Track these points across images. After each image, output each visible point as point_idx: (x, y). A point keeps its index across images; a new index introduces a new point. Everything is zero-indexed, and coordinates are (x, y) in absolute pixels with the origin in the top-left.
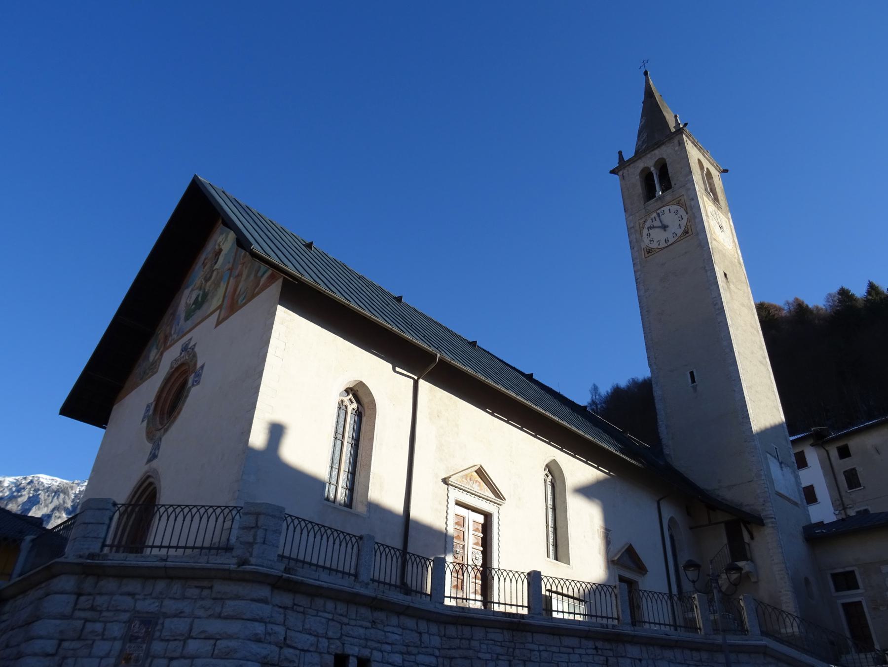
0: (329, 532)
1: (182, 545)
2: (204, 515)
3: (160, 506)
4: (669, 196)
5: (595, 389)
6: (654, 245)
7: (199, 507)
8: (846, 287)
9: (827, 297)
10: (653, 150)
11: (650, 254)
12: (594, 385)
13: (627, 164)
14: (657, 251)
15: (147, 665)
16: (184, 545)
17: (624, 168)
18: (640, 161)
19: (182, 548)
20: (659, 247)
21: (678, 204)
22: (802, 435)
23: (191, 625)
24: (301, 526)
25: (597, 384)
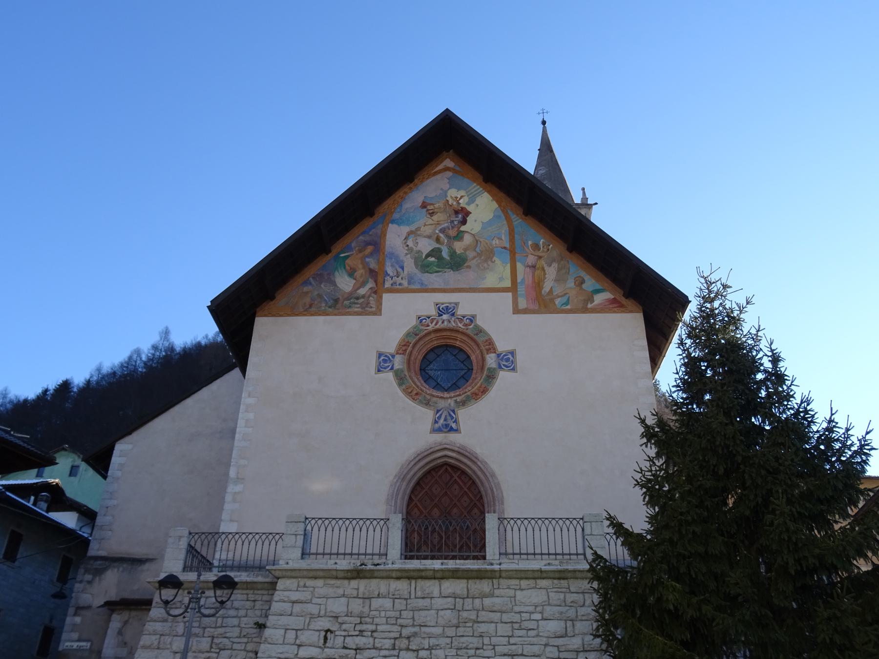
0: (568, 522)
1: (314, 552)
2: (266, 540)
3: (220, 534)
5: (166, 333)
7: (247, 534)
12: (167, 328)
15: (109, 647)
16: (322, 552)
24: (566, 525)
25: (170, 328)
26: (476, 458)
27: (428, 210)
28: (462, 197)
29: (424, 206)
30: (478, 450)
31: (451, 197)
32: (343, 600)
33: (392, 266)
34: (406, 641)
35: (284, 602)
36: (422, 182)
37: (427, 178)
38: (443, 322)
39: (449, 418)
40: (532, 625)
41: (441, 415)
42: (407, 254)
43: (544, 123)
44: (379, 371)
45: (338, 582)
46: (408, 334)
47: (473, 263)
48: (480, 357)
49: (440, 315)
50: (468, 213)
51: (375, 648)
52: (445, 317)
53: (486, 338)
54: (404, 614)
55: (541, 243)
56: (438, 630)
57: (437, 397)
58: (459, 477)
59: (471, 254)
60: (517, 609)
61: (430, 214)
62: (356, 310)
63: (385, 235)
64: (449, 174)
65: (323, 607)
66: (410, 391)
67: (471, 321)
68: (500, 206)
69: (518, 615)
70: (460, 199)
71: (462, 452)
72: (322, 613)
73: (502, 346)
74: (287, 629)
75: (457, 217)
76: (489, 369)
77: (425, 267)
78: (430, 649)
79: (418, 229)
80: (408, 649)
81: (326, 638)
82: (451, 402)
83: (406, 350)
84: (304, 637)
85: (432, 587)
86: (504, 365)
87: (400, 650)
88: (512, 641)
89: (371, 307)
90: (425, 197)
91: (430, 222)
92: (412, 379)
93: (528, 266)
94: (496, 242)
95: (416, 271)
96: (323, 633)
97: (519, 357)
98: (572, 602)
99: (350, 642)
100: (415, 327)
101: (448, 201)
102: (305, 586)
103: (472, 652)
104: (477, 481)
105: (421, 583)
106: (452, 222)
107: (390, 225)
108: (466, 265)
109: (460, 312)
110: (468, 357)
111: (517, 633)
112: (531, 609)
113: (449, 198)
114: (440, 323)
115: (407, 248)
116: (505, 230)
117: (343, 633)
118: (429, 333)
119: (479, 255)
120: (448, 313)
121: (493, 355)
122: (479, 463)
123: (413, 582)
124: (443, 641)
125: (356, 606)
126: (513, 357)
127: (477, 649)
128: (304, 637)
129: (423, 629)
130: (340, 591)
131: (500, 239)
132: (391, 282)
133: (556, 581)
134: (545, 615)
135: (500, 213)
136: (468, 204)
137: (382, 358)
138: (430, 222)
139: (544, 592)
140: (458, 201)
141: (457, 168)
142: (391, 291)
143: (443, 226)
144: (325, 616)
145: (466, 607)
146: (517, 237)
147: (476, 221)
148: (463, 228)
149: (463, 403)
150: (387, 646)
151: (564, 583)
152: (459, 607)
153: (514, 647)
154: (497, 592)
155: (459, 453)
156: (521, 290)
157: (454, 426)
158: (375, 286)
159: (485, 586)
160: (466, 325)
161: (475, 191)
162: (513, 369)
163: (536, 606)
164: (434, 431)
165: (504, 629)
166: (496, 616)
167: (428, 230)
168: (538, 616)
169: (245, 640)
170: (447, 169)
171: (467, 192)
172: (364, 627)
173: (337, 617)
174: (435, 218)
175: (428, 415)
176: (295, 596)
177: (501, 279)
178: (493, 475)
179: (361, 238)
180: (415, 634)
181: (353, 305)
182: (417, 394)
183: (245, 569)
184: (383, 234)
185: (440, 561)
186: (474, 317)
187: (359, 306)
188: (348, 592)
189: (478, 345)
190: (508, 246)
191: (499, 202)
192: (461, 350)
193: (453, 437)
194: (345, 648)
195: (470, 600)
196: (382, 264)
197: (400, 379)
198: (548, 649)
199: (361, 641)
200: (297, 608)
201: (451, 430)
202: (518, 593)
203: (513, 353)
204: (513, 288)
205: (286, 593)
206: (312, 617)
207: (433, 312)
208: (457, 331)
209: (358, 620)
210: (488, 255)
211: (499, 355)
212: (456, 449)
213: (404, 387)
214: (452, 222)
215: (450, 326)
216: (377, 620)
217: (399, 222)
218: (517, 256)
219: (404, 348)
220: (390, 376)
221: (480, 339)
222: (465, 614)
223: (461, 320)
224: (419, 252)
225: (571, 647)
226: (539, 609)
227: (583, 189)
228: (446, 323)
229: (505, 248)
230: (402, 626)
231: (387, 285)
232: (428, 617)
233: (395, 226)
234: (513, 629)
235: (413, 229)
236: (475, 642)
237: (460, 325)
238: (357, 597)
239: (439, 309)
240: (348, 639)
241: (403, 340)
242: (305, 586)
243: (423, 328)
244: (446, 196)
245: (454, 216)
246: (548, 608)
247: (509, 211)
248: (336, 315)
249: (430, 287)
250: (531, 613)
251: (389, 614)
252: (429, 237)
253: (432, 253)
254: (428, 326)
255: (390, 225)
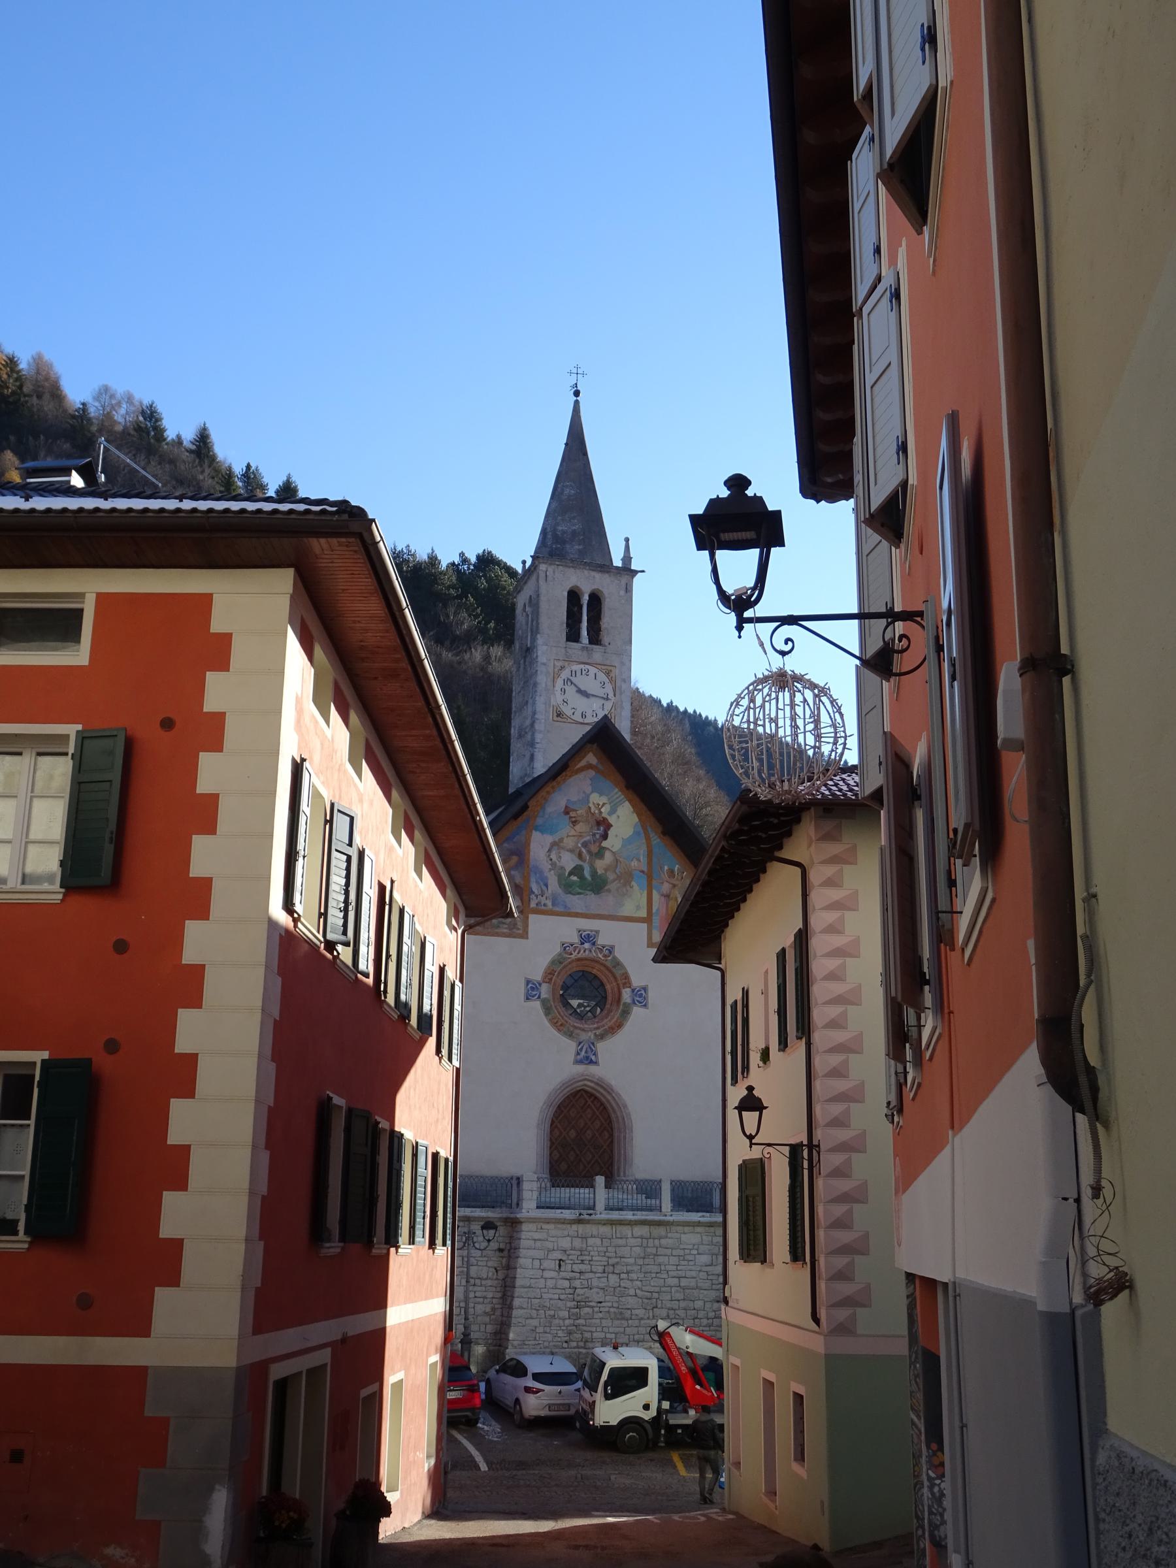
4: (597, 653)
6: (567, 710)
8: (161, 408)
9: (100, 390)
10: (593, 570)
11: (559, 719)
13: (557, 563)
14: (569, 720)
17: (551, 564)
18: (572, 570)
19: (651, 934)
20: (572, 717)
21: (608, 674)
22: (631, 1519)
23: (929, 1009)
26: (612, 1090)
27: (571, 817)
28: (604, 804)
29: (567, 812)
30: (613, 1083)
31: (594, 803)
32: (569, 1239)
33: (537, 882)
34: (611, 1268)
35: (529, 1239)
36: (564, 780)
37: (570, 776)
38: (584, 951)
39: (589, 1050)
40: (690, 1258)
41: (582, 1047)
42: (550, 870)
43: (577, 393)
44: (528, 999)
45: (564, 1226)
46: (553, 962)
47: (613, 886)
48: (616, 989)
49: (582, 944)
50: (609, 826)
51: (591, 1272)
52: (587, 945)
53: (623, 971)
54: (609, 1249)
55: (676, 869)
56: (632, 1261)
57: (580, 1029)
58: (592, 1102)
59: (611, 876)
60: (682, 1247)
61: (573, 822)
62: (505, 931)
63: (529, 845)
64: (592, 773)
65: (556, 1244)
66: (555, 1021)
67: (610, 952)
68: (640, 819)
69: (682, 1251)
70: (602, 807)
71: (600, 1083)
72: (555, 1248)
73: (636, 982)
74: (533, 1259)
75: (599, 829)
76: (625, 1004)
77: (568, 887)
78: (628, 1273)
79: (561, 840)
80: (613, 1273)
81: (560, 1266)
82: (591, 1035)
83: (551, 979)
84: (546, 1264)
85: (627, 1231)
86: (638, 1001)
87: (609, 1273)
88: (679, 1268)
89: (519, 929)
90: (568, 800)
91: (573, 833)
92: (557, 1009)
93: (662, 895)
94: (634, 864)
95: (560, 891)
96: (557, 1262)
97: (651, 994)
98: (717, 1243)
99: (576, 1268)
100: (560, 954)
101: (590, 808)
102: (541, 1228)
103: (654, 1275)
104: (608, 1105)
105: (619, 1228)
106: (594, 835)
107: (534, 831)
108: (606, 888)
109: (601, 941)
110: (602, 985)
111: (683, 1263)
112: (691, 1247)
113: (591, 805)
114: (582, 951)
115: (550, 862)
116: (643, 851)
117: (571, 1262)
118: (573, 961)
119: (619, 878)
120: (589, 942)
121: (628, 990)
122: (614, 1095)
123: (614, 1227)
124: (636, 1268)
125: (578, 1243)
126: (645, 992)
127: (657, 1273)
128: (546, 1264)
129: (622, 1259)
130: (566, 1233)
131: (639, 860)
132: (536, 902)
133: (707, 1228)
134: (700, 1251)
135: (640, 829)
136: (610, 814)
137: (530, 985)
138: (573, 833)
139: (699, 1236)
140: (600, 809)
141: (600, 767)
142: (537, 912)
143: (585, 839)
144: (558, 1250)
145: (649, 1245)
146: (655, 860)
147: (616, 836)
148: (605, 844)
149: (601, 1037)
150: (600, 1271)
151: (712, 1229)
152: (645, 1245)
153: (680, 1272)
154: (669, 1235)
155: (597, 1084)
156: (656, 921)
157: (593, 1058)
158: (521, 904)
159: (661, 1231)
160: (605, 956)
161: (617, 798)
162: (645, 1006)
163: (694, 1245)
164: (578, 1062)
165: (674, 1260)
166: (668, 1252)
167: (569, 843)
168: (695, 1252)
169: (486, 1259)
170: (589, 766)
171: (609, 799)
172: (584, 1258)
173: (565, 1251)
174: (578, 827)
175: (570, 1046)
176: (537, 1236)
177: (638, 908)
178: (625, 1106)
179: (506, 845)
180: (617, 1263)
181: (501, 925)
182: (561, 1025)
183: (510, 1224)
184: (527, 844)
185: (632, 1212)
186: (613, 947)
187: (506, 926)
188: (571, 1233)
189: (615, 978)
190: (645, 869)
191: (639, 815)
192: (596, 977)
193: (592, 1069)
194: (572, 1271)
195: (652, 1240)
196: (526, 879)
197: (547, 1010)
198: (701, 1273)
199: (583, 1267)
200: (538, 1244)
201: (591, 1062)
202: (682, 1235)
203: (645, 989)
204: (648, 920)
205: (530, 1234)
206: (549, 1251)
207: (576, 940)
208: (597, 962)
209: (579, 1253)
210: (627, 878)
211: (633, 990)
212: (596, 1080)
213: (550, 1017)
214: (594, 835)
215: (590, 955)
216: (592, 1253)
217: (542, 829)
218: (654, 883)
219: (550, 977)
220: (537, 1004)
221: (618, 973)
222: (649, 1250)
223: (601, 951)
224: (562, 868)
225: (714, 1272)
226: (696, 1247)
227: (627, 540)
228: (587, 952)
229: (643, 872)
230: (608, 1257)
231: (533, 905)
232: (625, 1251)
233: (538, 833)
234: (679, 1260)
235: (557, 840)
236: (655, 1269)
237: (600, 956)
238: (578, 1237)
239: (581, 935)
240: (574, 1266)
241: (548, 967)
242: (541, 1228)
243: (567, 956)
244: (588, 802)
245: (596, 828)
246: (701, 1246)
247: (648, 827)
248: (485, 935)
249: (573, 910)
250: (690, 1250)
251: (600, 1249)
252: (571, 851)
253: (578, 870)
254: (572, 954)
255: (534, 831)
